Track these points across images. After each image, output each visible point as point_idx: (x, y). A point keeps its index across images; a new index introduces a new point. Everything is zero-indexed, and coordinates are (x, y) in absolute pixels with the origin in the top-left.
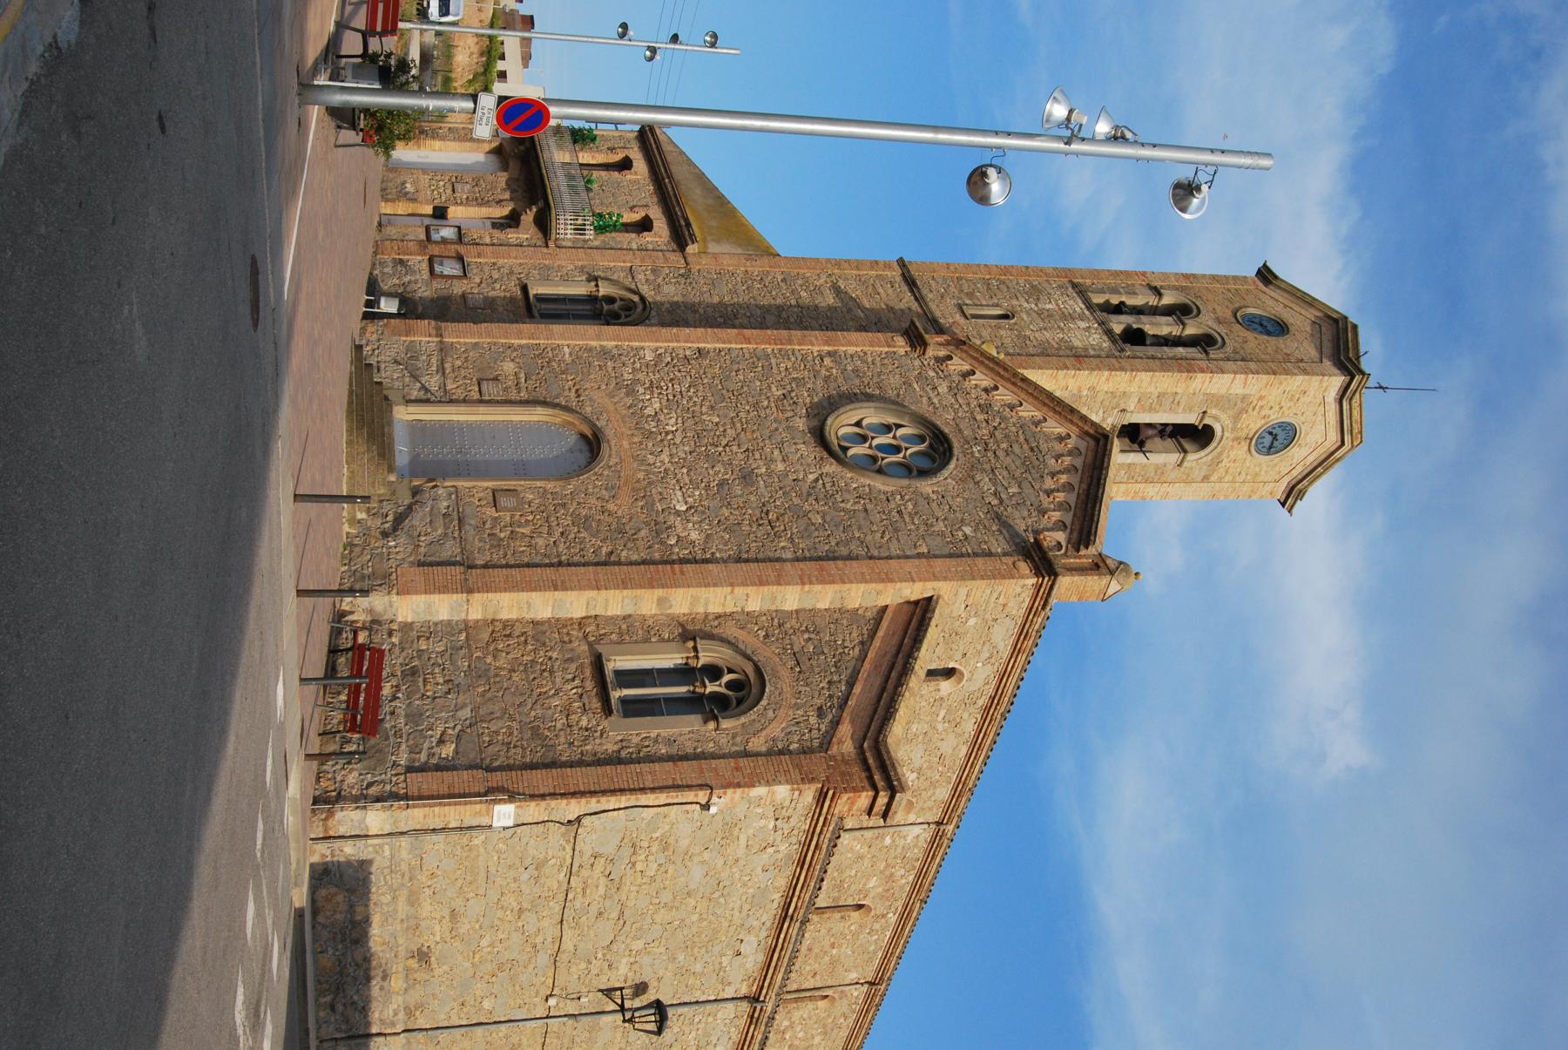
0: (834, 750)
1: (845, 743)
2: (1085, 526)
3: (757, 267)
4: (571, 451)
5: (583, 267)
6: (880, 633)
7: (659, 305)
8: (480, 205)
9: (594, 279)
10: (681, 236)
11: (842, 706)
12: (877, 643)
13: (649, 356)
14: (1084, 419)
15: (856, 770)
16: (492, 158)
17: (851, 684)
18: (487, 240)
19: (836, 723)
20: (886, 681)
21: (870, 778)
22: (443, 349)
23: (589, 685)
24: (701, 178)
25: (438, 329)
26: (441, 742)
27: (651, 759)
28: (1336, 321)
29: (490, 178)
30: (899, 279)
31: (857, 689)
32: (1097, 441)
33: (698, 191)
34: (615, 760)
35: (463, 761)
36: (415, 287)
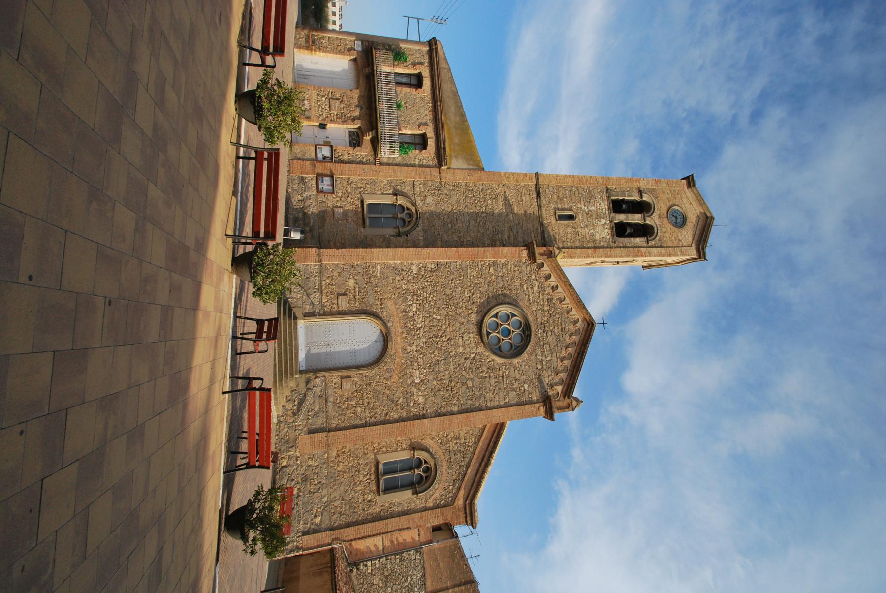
0: (456, 504)
1: (460, 502)
2: (568, 391)
3: (472, 179)
4: (376, 341)
5: (391, 182)
6: (483, 439)
7: (424, 213)
8: (344, 122)
9: (395, 194)
10: (440, 158)
11: (462, 480)
12: (480, 444)
13: (415, 269)
14: (587, 312)
15: (462, 514)
16: (352, 63)
17: (467, 468)
18: (346, 158)
19: (459, 489)
20: (480, 465)
21: (466, 517)
22: (322, 269)
23: (373, 477)
24: (459, 107)
25: (319, 255)
26: (316, 516)
27: (392, 516)
28: (707, 217)
29: (350, 93)
30: (533, 188)
31: (469, 471)
32: (589, 324)
33: (453, 109)
34: (378, 518)
35: (324, 526)
36: (308, 203)
